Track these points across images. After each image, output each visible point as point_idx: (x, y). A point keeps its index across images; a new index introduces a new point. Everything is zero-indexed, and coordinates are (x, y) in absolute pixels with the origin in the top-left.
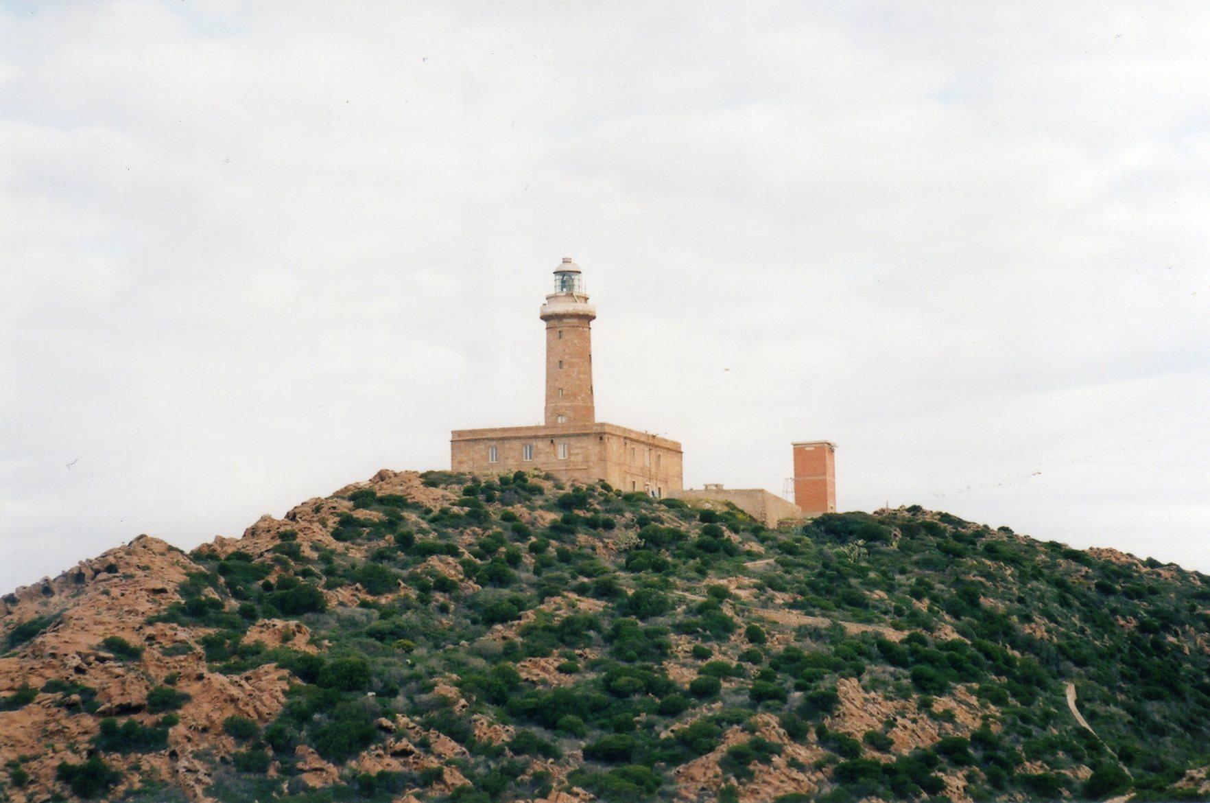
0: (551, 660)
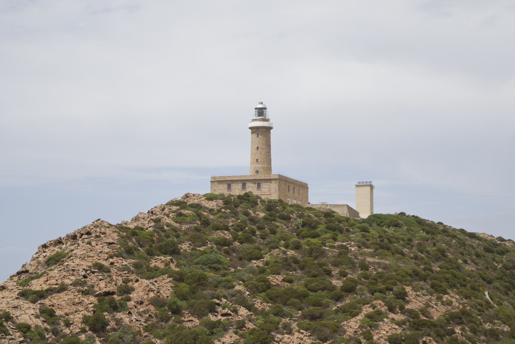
0: (280, 276)
